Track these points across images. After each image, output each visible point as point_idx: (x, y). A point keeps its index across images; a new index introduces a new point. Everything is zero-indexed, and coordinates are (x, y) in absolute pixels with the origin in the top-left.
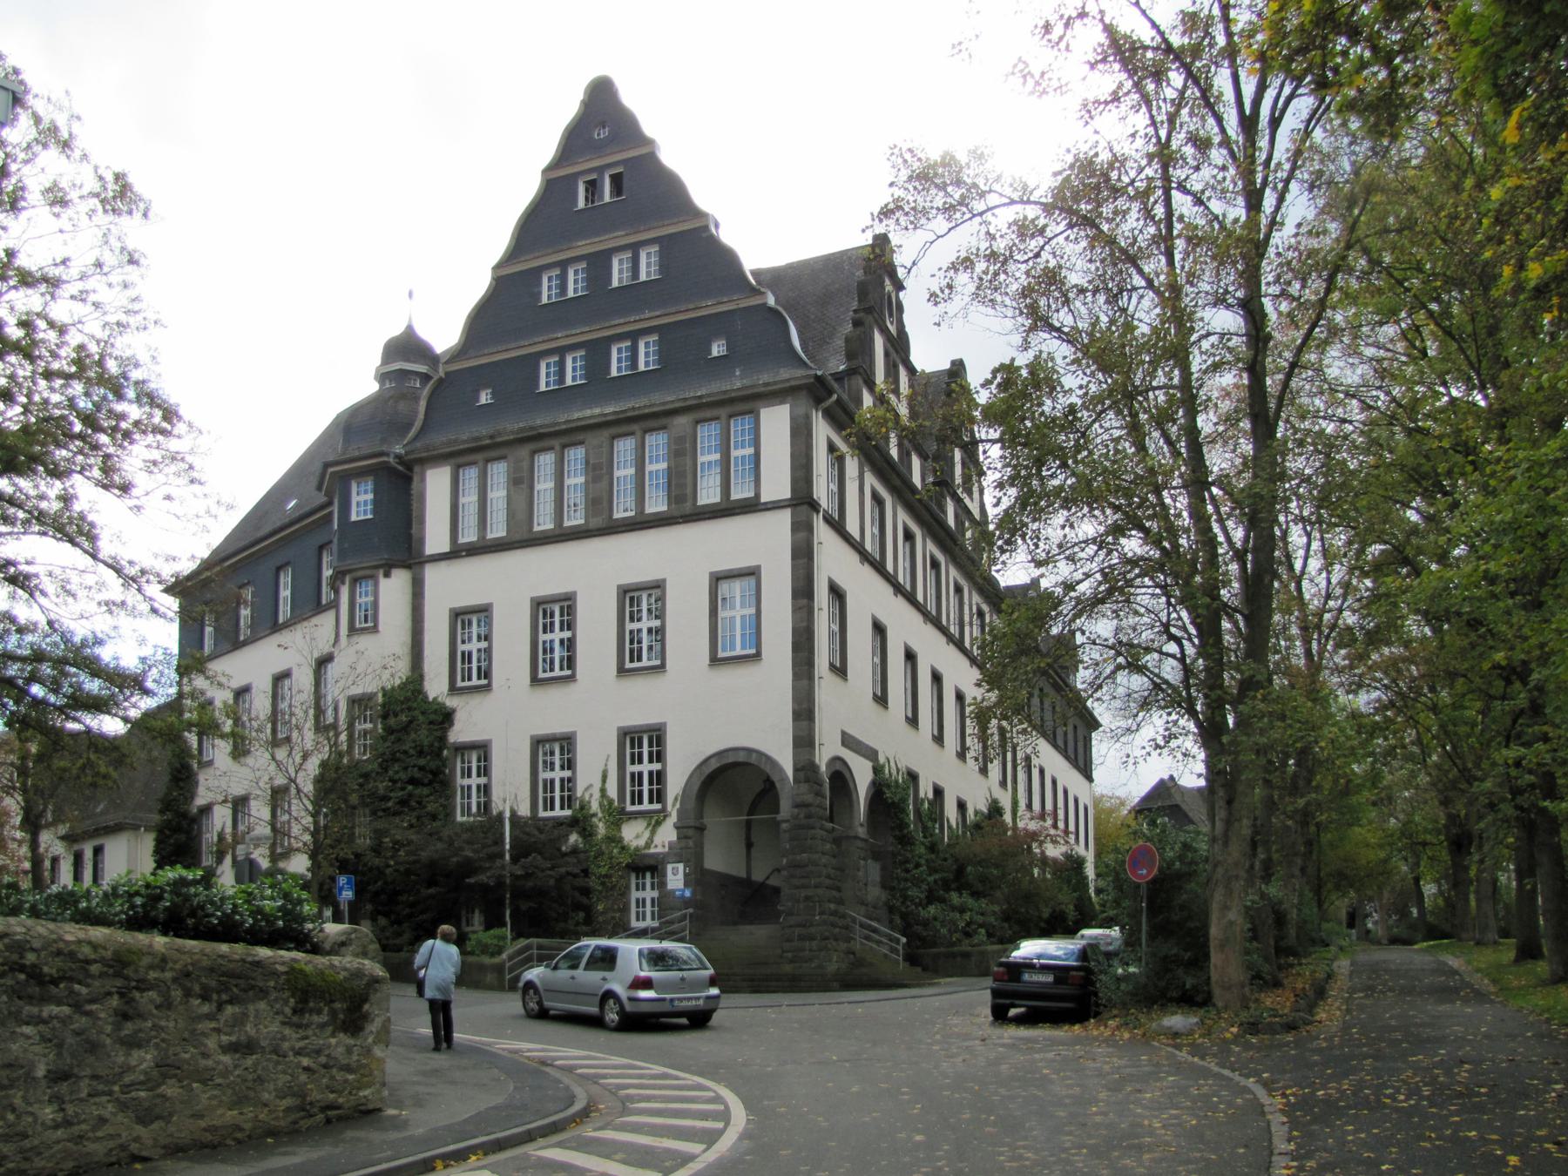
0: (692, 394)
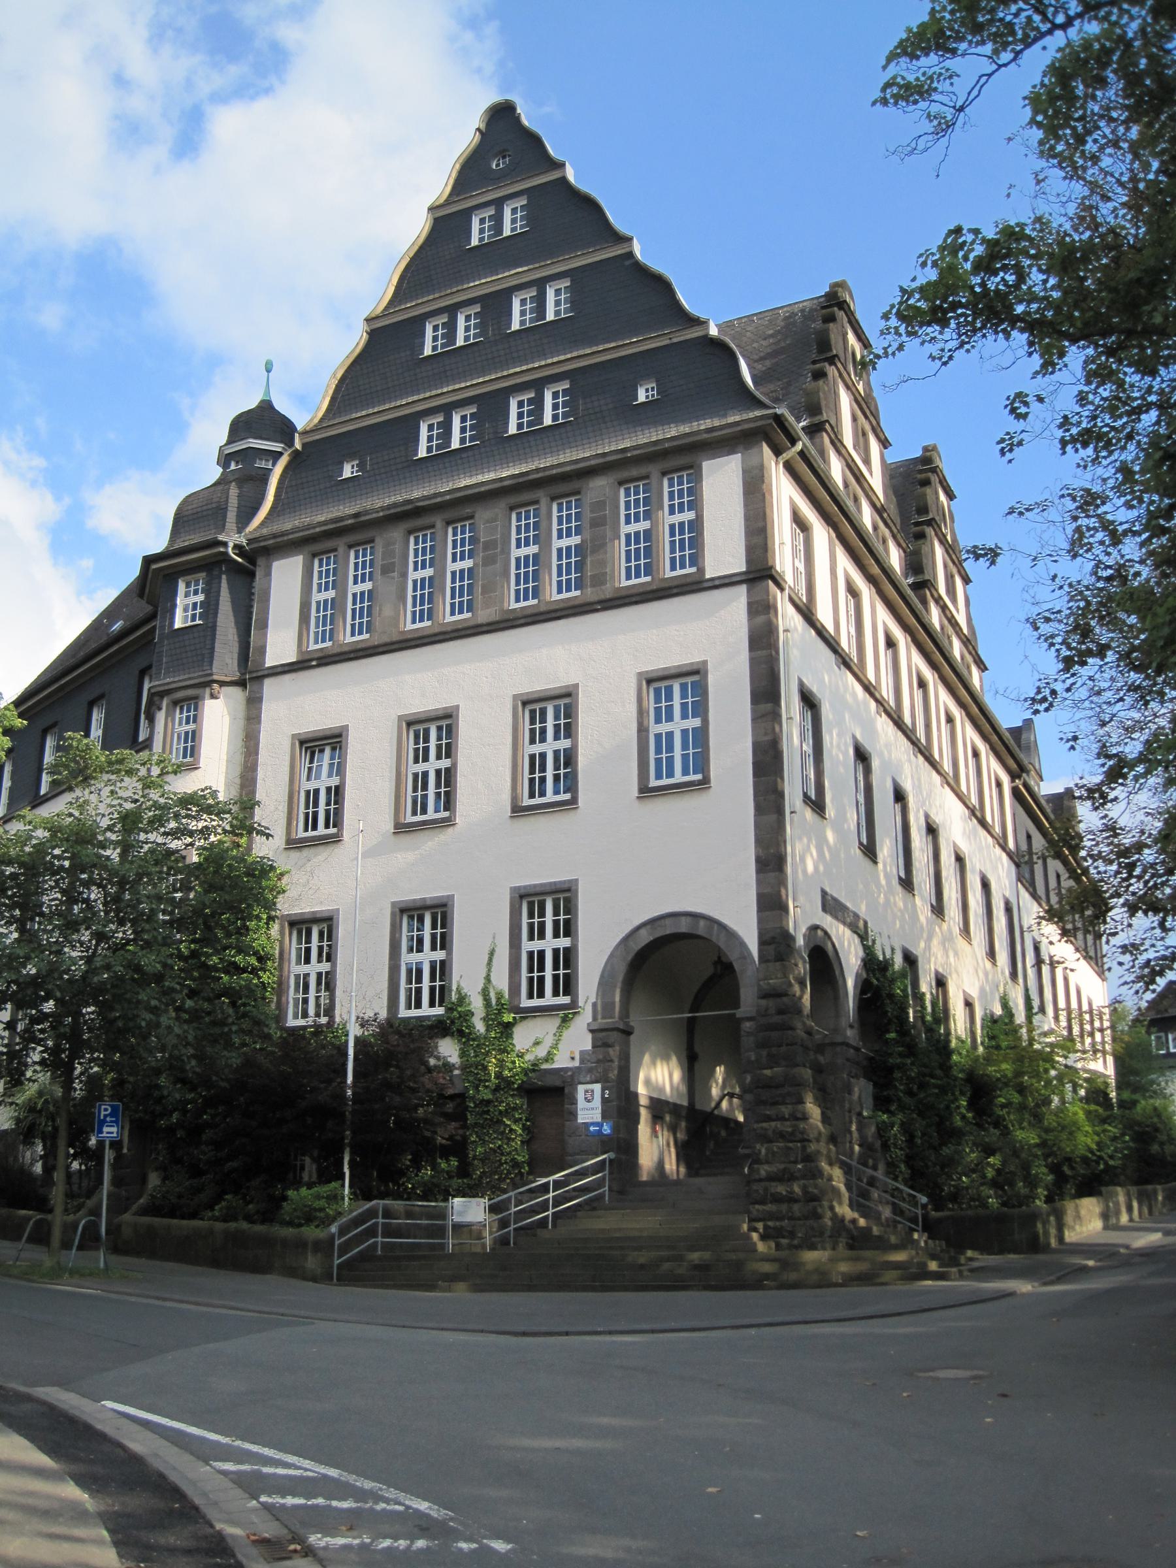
0: (613, 448)
